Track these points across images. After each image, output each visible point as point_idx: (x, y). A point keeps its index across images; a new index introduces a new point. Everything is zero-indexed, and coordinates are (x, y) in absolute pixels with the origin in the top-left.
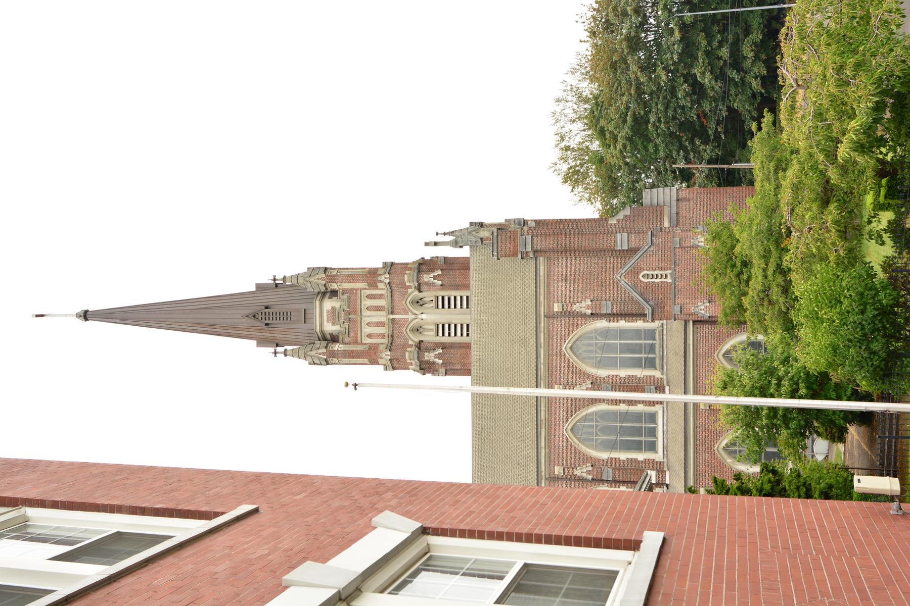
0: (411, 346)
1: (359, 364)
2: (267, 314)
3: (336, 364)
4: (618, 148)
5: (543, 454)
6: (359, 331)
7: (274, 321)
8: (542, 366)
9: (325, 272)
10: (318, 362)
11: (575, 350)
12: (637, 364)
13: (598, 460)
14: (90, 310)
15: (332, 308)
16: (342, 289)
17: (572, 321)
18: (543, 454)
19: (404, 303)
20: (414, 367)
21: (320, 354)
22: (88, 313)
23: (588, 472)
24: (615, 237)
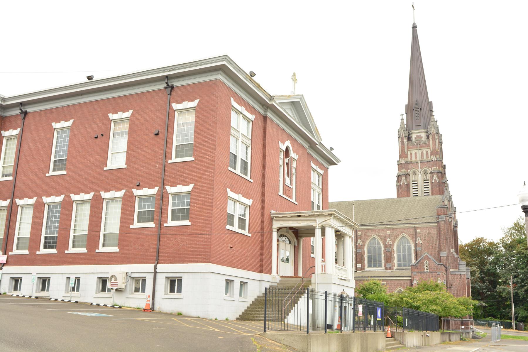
1: (399, 150)
2: (418, 109)
3: (399, 141)
4: (522, 250)
5: (365, 228)
7: (415, 113)
9: (436, 133)
10: (399, 134)
11: (403, 238)
12: (399, 260)
13: (364, 247)
15: (422, 137)
16: (430, 141)
17: (414, 236)
18: (365, 228)
19: (425, 167)
20: (399, 173)
21: (402, 134)
22: (415, 28)
23: (359, 244)
24: (445, 251)
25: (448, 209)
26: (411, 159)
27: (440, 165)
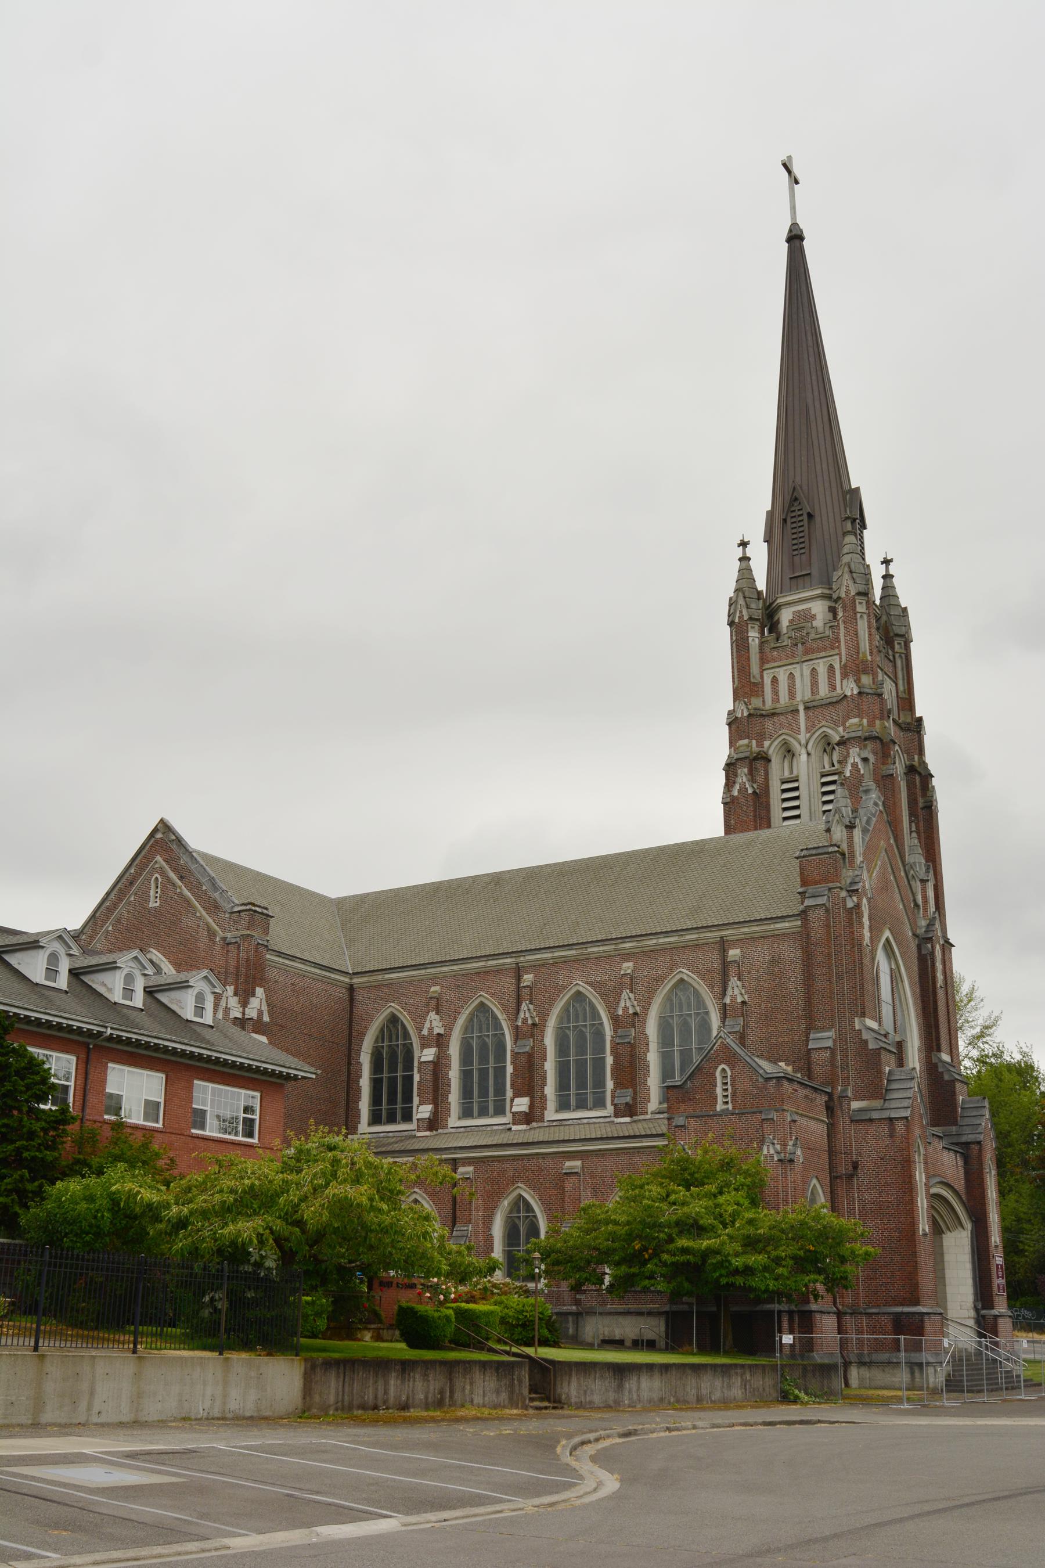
0: (760, 744)
3: (732, 639)
6: (779, 664)
8: (654, 941)
9: (859, 594)
14: (804, 243)
15: (814, 617)
16: (838, 625)
17: (718, 978)
19: (824, 723)
21: (741, 612)
24: (829, 1029)
25: (844, 859)
26: (776, 700)
27: (877, 712)
